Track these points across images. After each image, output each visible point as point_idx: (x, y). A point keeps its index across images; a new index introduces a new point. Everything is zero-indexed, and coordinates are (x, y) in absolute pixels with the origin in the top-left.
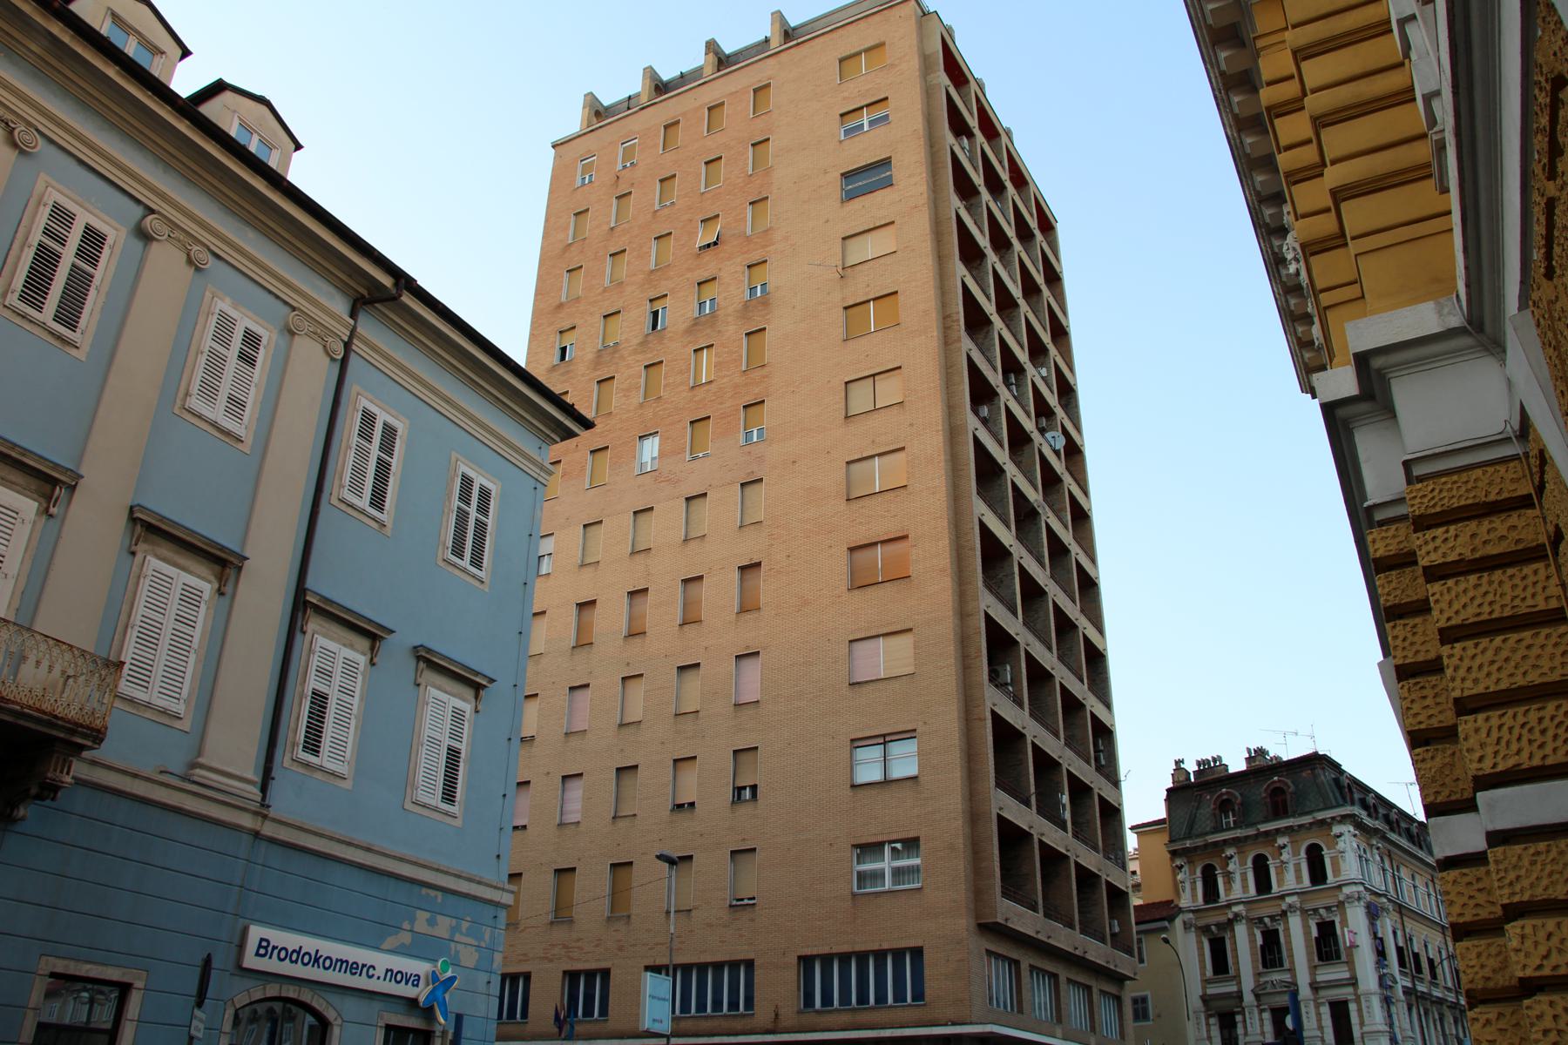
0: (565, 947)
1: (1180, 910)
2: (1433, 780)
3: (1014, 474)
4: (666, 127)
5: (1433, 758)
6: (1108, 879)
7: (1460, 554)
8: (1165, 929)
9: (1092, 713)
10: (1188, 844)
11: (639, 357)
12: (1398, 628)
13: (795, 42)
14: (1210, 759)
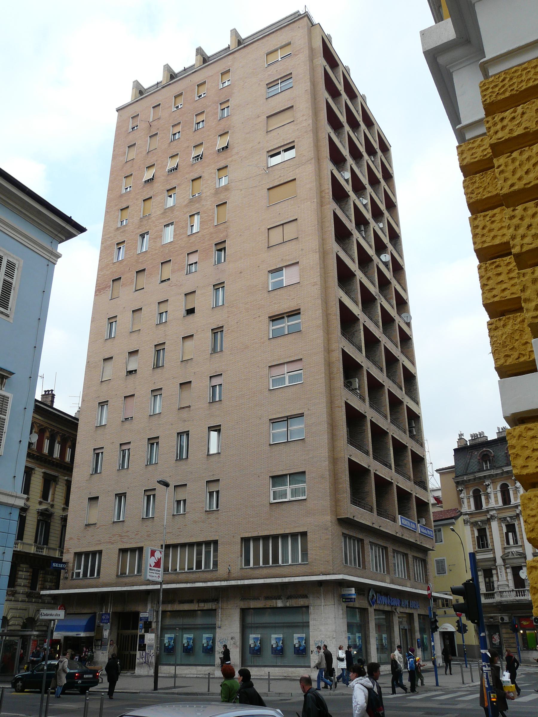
0: (120, 536)
1: (461, 514)
2: (504, 345)
3: (361, 277)
4: (175, 97)
5: (504, 326)
6: (417, 496)
7: (526, 128)
8: (453, 524)
9: (407, 406)
10: (465, 478)
11: (162, 221)
12: (479, 219)
13: (243, 46)
14: (478, 433)
